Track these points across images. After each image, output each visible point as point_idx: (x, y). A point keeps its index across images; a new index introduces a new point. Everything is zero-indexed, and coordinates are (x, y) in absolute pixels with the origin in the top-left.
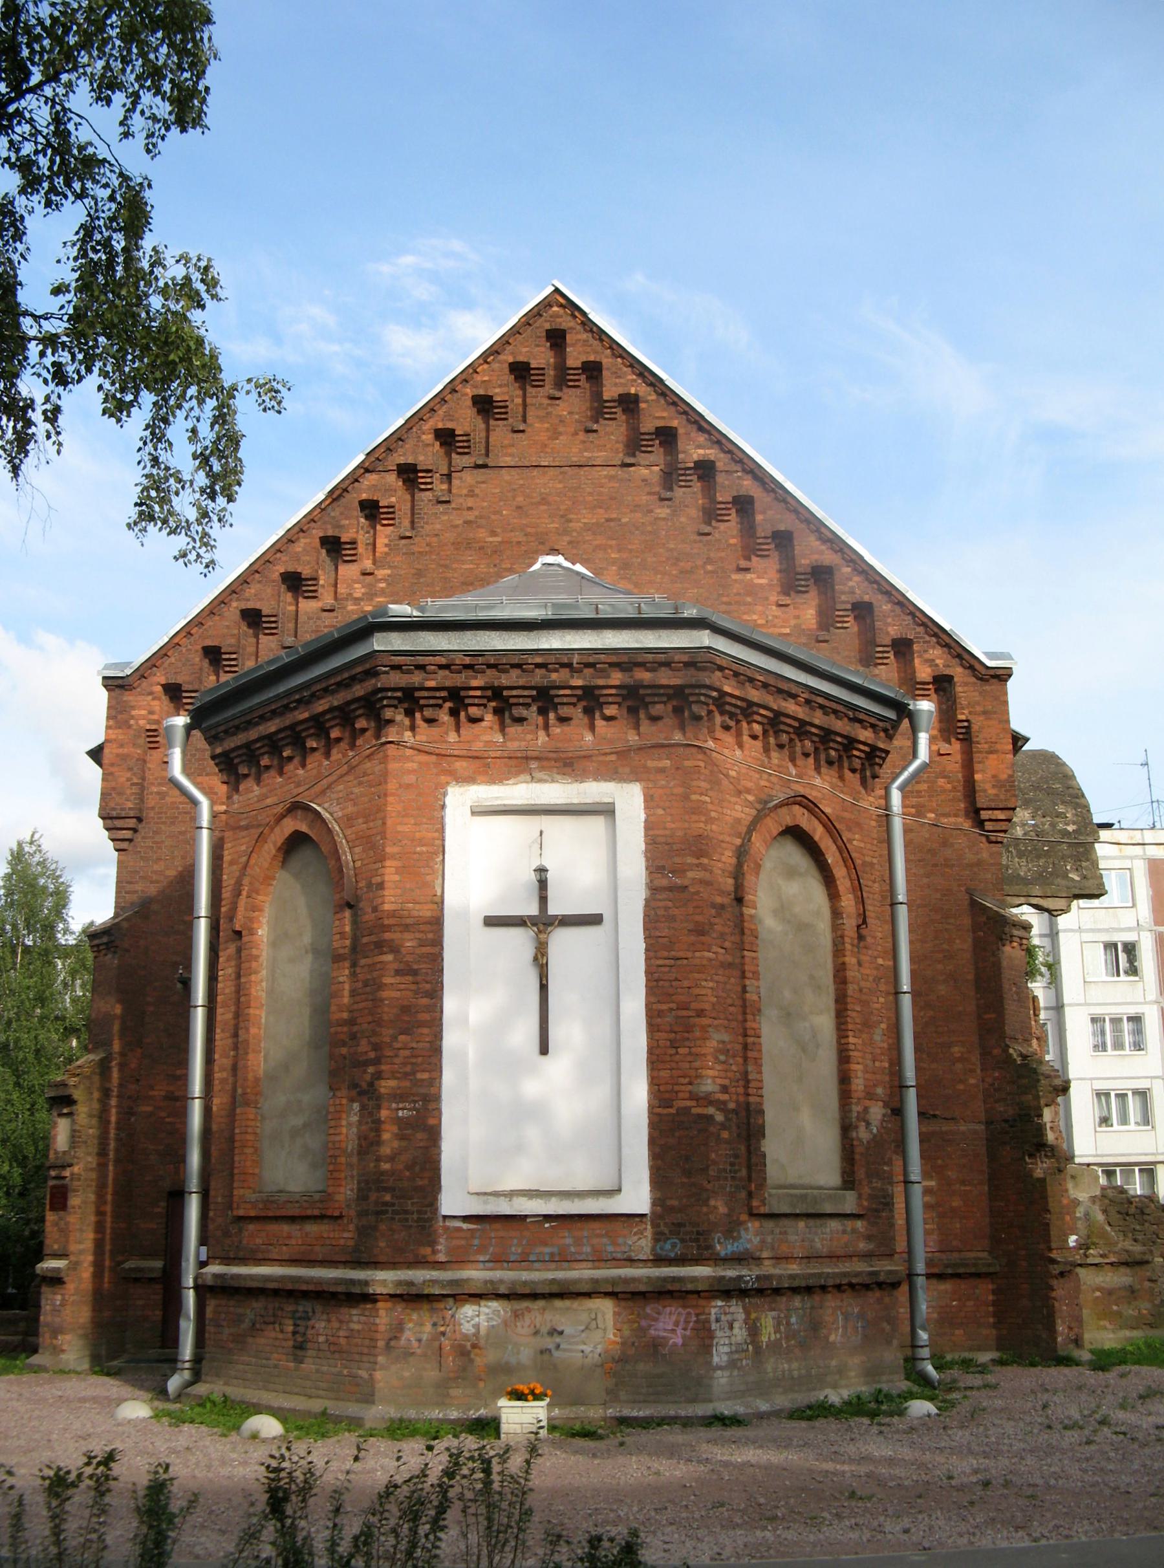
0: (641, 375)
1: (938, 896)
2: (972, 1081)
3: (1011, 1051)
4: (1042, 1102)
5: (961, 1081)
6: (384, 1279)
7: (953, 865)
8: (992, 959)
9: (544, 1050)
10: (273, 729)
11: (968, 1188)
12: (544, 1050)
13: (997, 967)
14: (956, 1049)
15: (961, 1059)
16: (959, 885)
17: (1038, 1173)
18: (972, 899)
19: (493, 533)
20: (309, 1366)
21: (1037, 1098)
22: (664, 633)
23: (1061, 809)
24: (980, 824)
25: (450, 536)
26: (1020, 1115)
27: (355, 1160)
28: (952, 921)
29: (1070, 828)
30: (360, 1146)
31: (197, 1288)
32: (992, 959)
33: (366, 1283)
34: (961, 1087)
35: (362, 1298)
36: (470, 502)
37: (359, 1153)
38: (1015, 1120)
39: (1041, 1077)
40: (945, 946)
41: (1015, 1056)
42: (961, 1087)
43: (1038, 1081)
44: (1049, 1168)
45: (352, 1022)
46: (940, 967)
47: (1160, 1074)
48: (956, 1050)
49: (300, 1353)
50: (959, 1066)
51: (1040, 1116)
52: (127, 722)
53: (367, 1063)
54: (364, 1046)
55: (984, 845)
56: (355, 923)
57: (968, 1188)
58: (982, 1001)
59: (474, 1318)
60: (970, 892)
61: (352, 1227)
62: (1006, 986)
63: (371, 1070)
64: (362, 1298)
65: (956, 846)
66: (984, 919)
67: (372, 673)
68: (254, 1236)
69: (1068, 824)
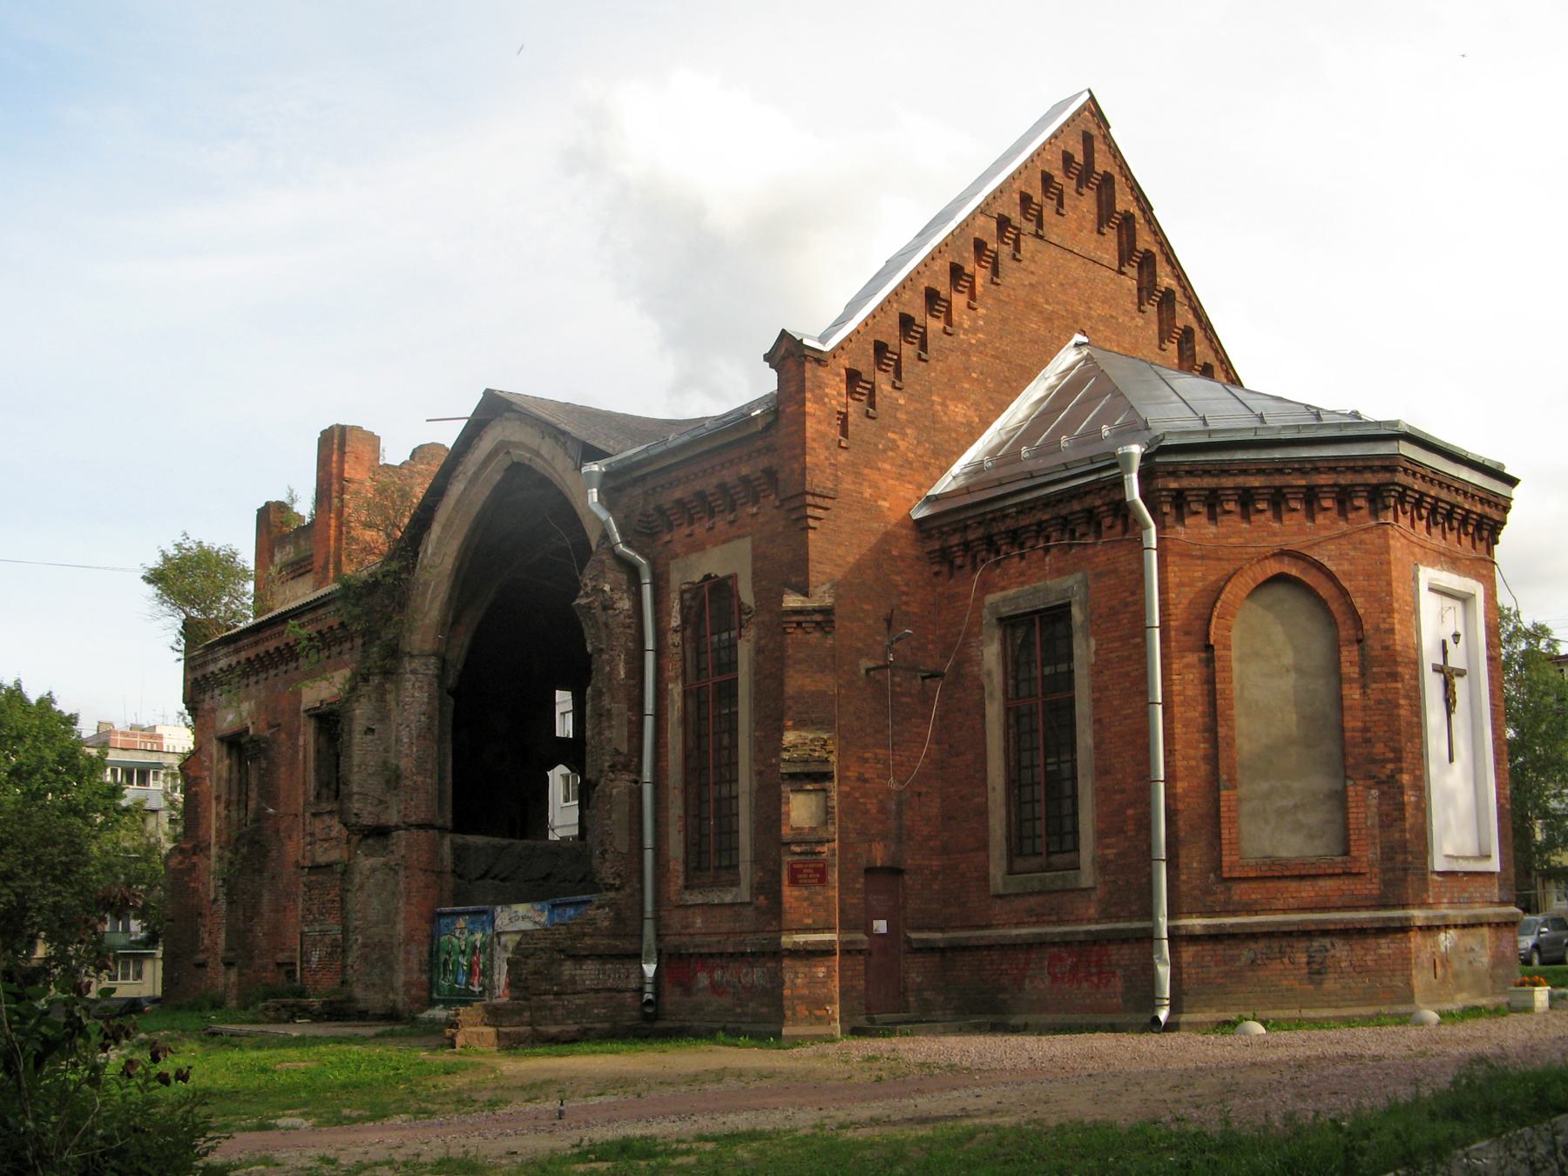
0: (1137, 199)
6: (1418, 915)
9: (1451, 760)
10: (1257, 484)
12: (1451, 760)
17: (762, 898)
19: (1047, 302)
20: (1330, 984)
22: (1498, 483)
25: (1022, 293)
27: (1376, 832)
30: (1381, 821)
31: (1171, 938)
33: (1407, 919)
35: (1404, 928)
36: (1032, 267)
37: (1381, 827)
45: (1365, 729)
49: (1317, 977)
52: (822, 399)
53: (1385, 761)
54: (1379, 748)
56: (1363, 655)
59: (1446, 940)
61: (1376, 881)
63: (1390, 766)
64: (1404, 928)
67: (1391, 469)
68: (1239, 892)
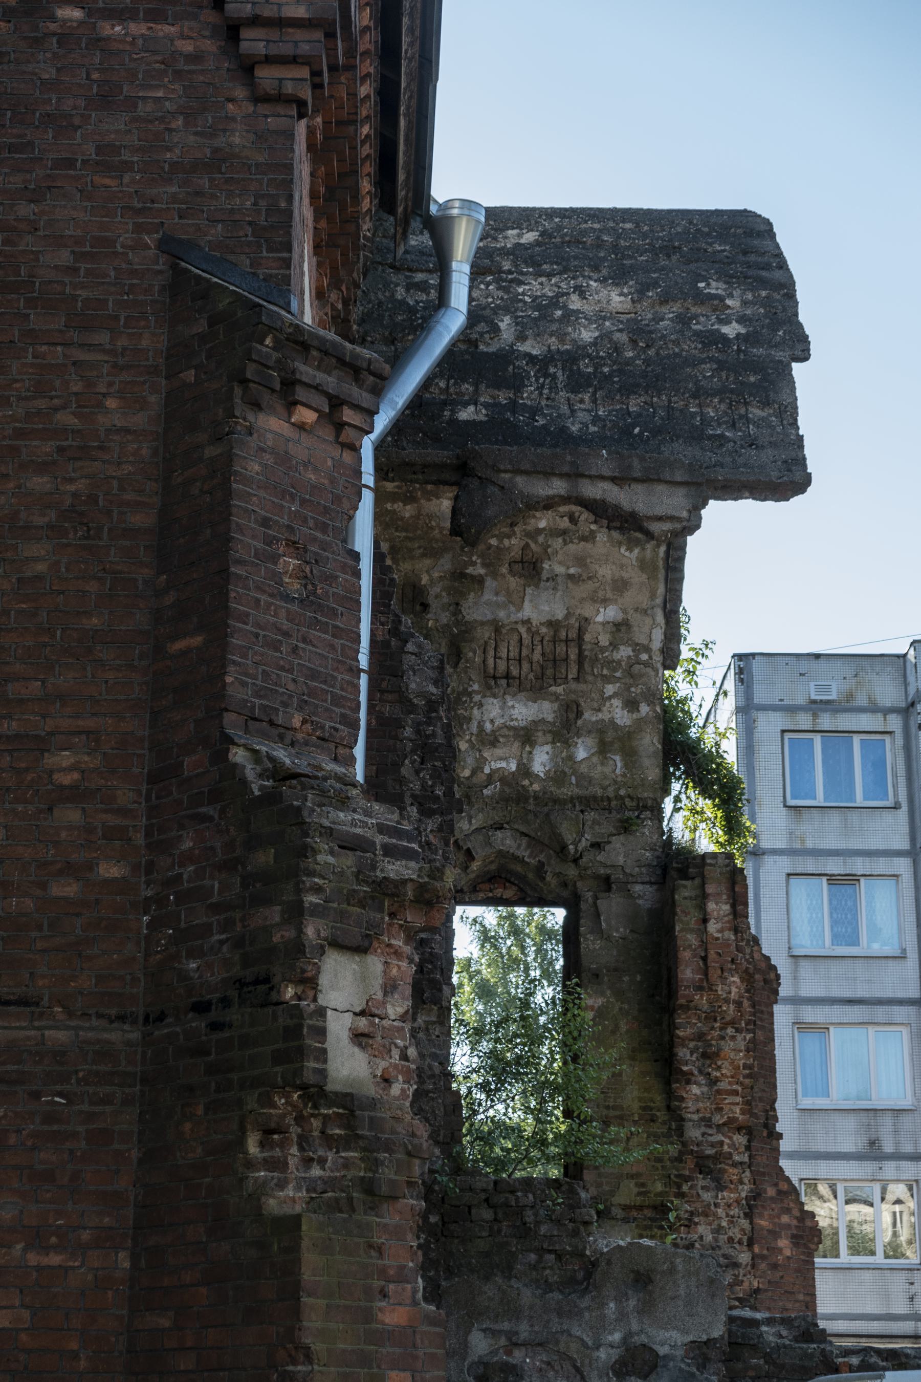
1: (64, 257)
2: (111, 870)
3: (238, 755)
4: (311, 931)
5: (68, 870)
7: (127, 166)
8: (210, 452)
11: (55, 1259)
13: (222, 473)
14: (66, 758)
15: (74, 795)
16: (139, 228)
17: (287, 1199)
18: (174, 267)
21: (296, 913)
23: (716, 288)
24: (247, 68)
26: (240, 983)
28: (103, 338)
29: (731, 330)
32: (210, 452)
34: (66, 889)
38: (225, 1002)
39: (319, 842)
40: (66, 419)
41: (250, 772)
42: (66, 889)
43: (305, 851)
44: (330, 1183)
46: (39, 483)
47: (913, 993)
48: (64, 764)
50: (71, 815)
51: (310, 983)
55: (239, 103)
57: (55, 1259)
58: (170, 599)
60: (171, 247)
62: (247, 542)
65: (143, 109)
66: (201, 326)
69: (727, 322)
